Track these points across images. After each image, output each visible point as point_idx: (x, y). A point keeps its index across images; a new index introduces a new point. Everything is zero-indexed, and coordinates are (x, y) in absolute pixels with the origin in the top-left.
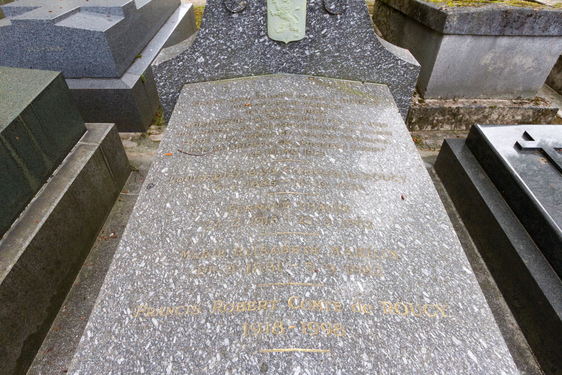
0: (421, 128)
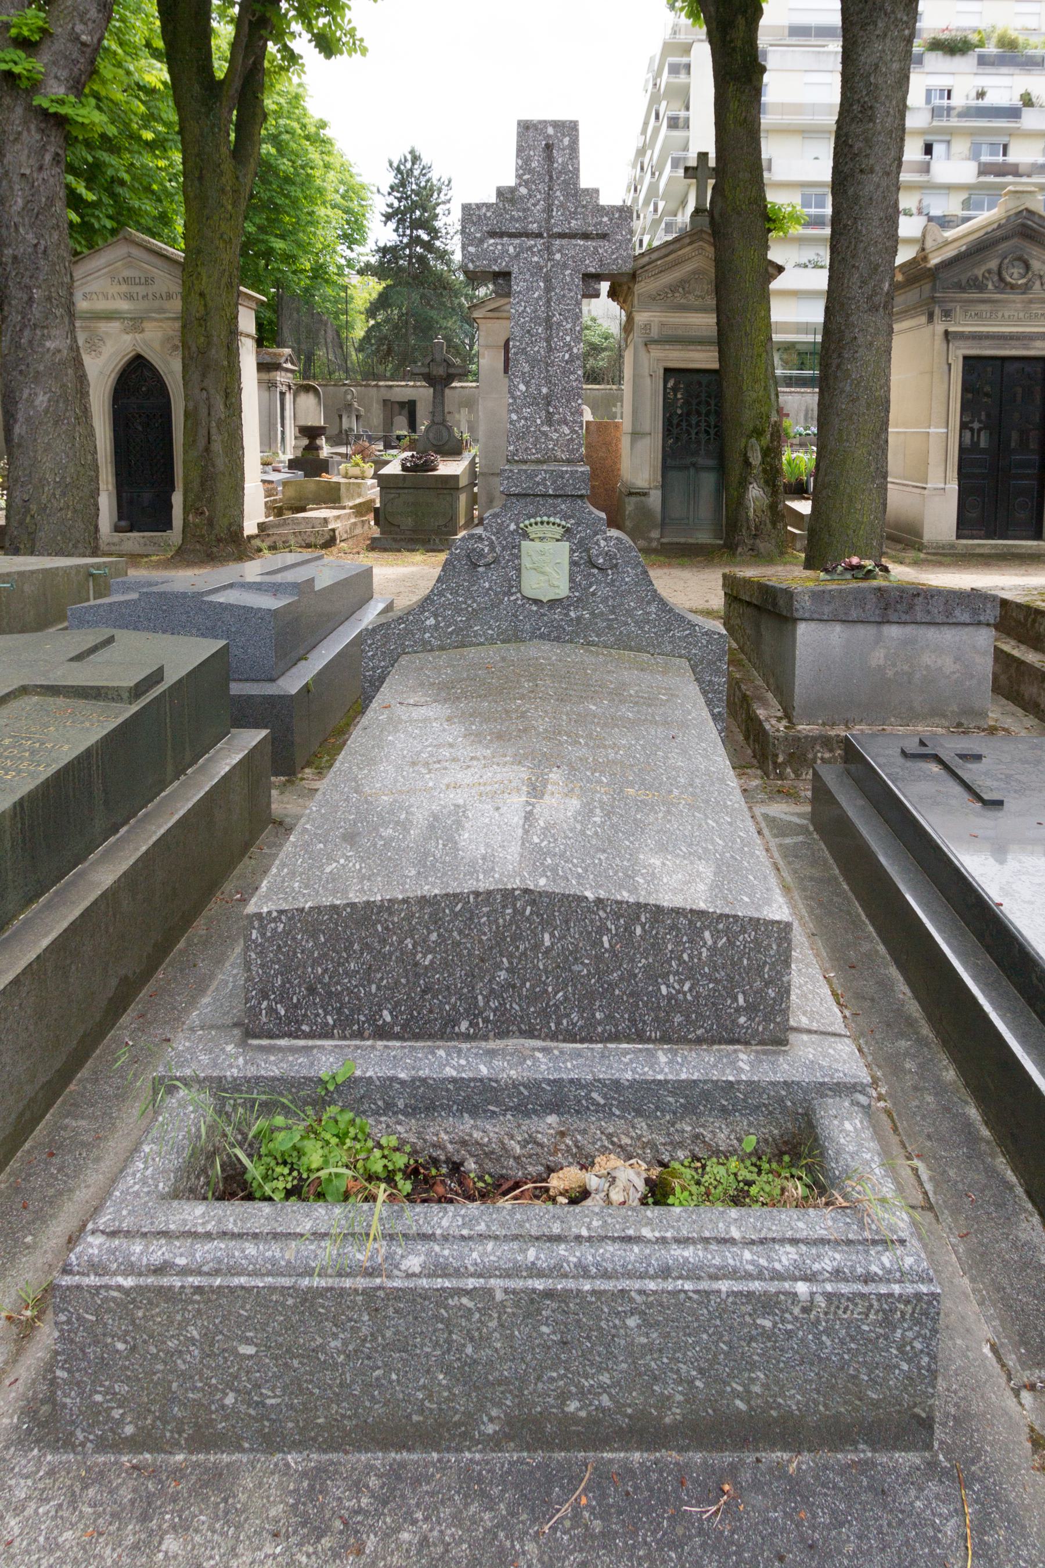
0: (798, 776)
